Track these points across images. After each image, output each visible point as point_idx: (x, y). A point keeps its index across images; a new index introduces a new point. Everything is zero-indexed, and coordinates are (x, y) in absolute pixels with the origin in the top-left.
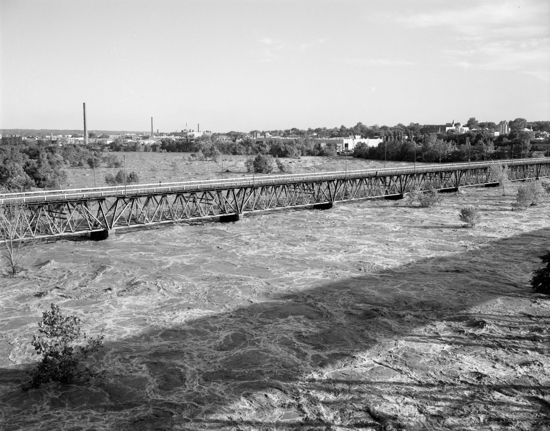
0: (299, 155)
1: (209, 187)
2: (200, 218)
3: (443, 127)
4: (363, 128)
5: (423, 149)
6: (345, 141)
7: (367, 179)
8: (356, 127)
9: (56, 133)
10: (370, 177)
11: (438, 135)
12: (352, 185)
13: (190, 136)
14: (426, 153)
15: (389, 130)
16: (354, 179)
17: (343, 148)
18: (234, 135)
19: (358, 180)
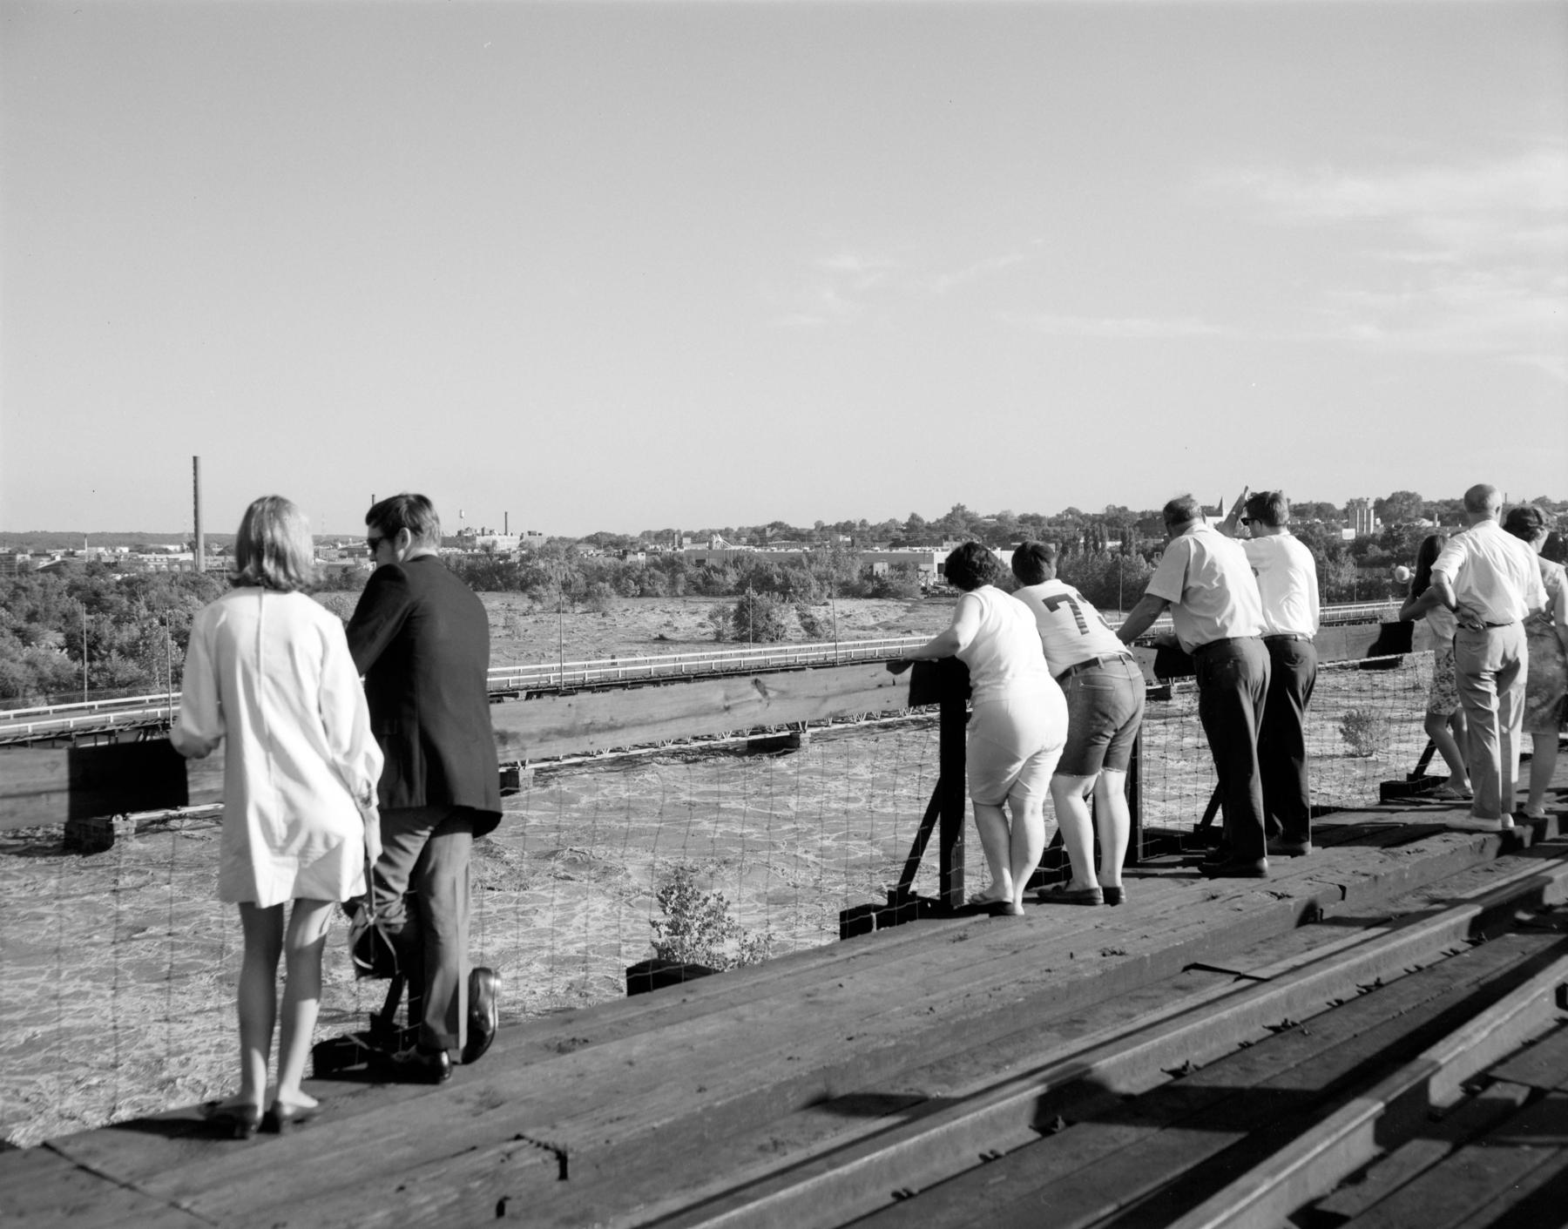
9: (112, 540)
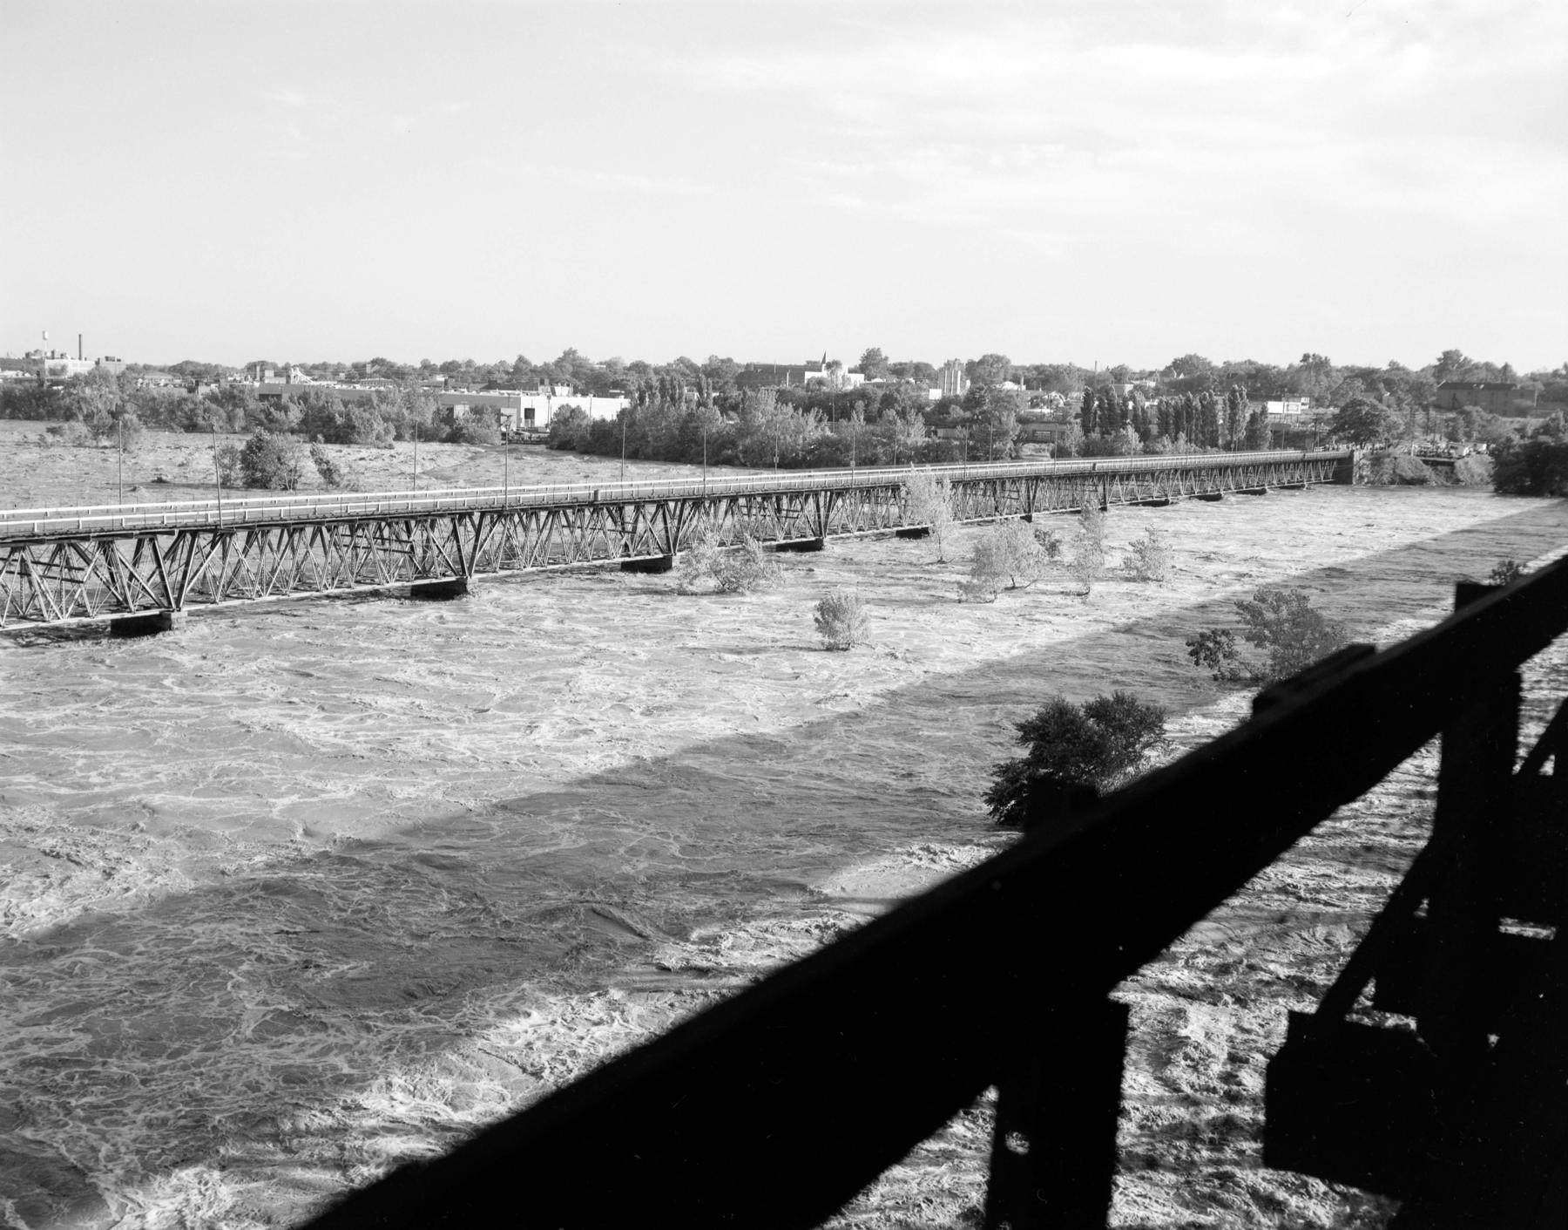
0: (390, 439)
1: (73, 528)
2: (42, 624)
3: (797, 372)
4: (581, 366)
5: (739, 430)
6: (527, 401)
7: (569, 512)
8: (559, 363)
10: (578, 506)
11: (781, 393)
12: (526, 528)
13: (53, 372)
14: (748, 441)
15: (652, 375)
16: (532, 511)
17: (519, 420)
18: (192, 374)
19: (543, 514)
